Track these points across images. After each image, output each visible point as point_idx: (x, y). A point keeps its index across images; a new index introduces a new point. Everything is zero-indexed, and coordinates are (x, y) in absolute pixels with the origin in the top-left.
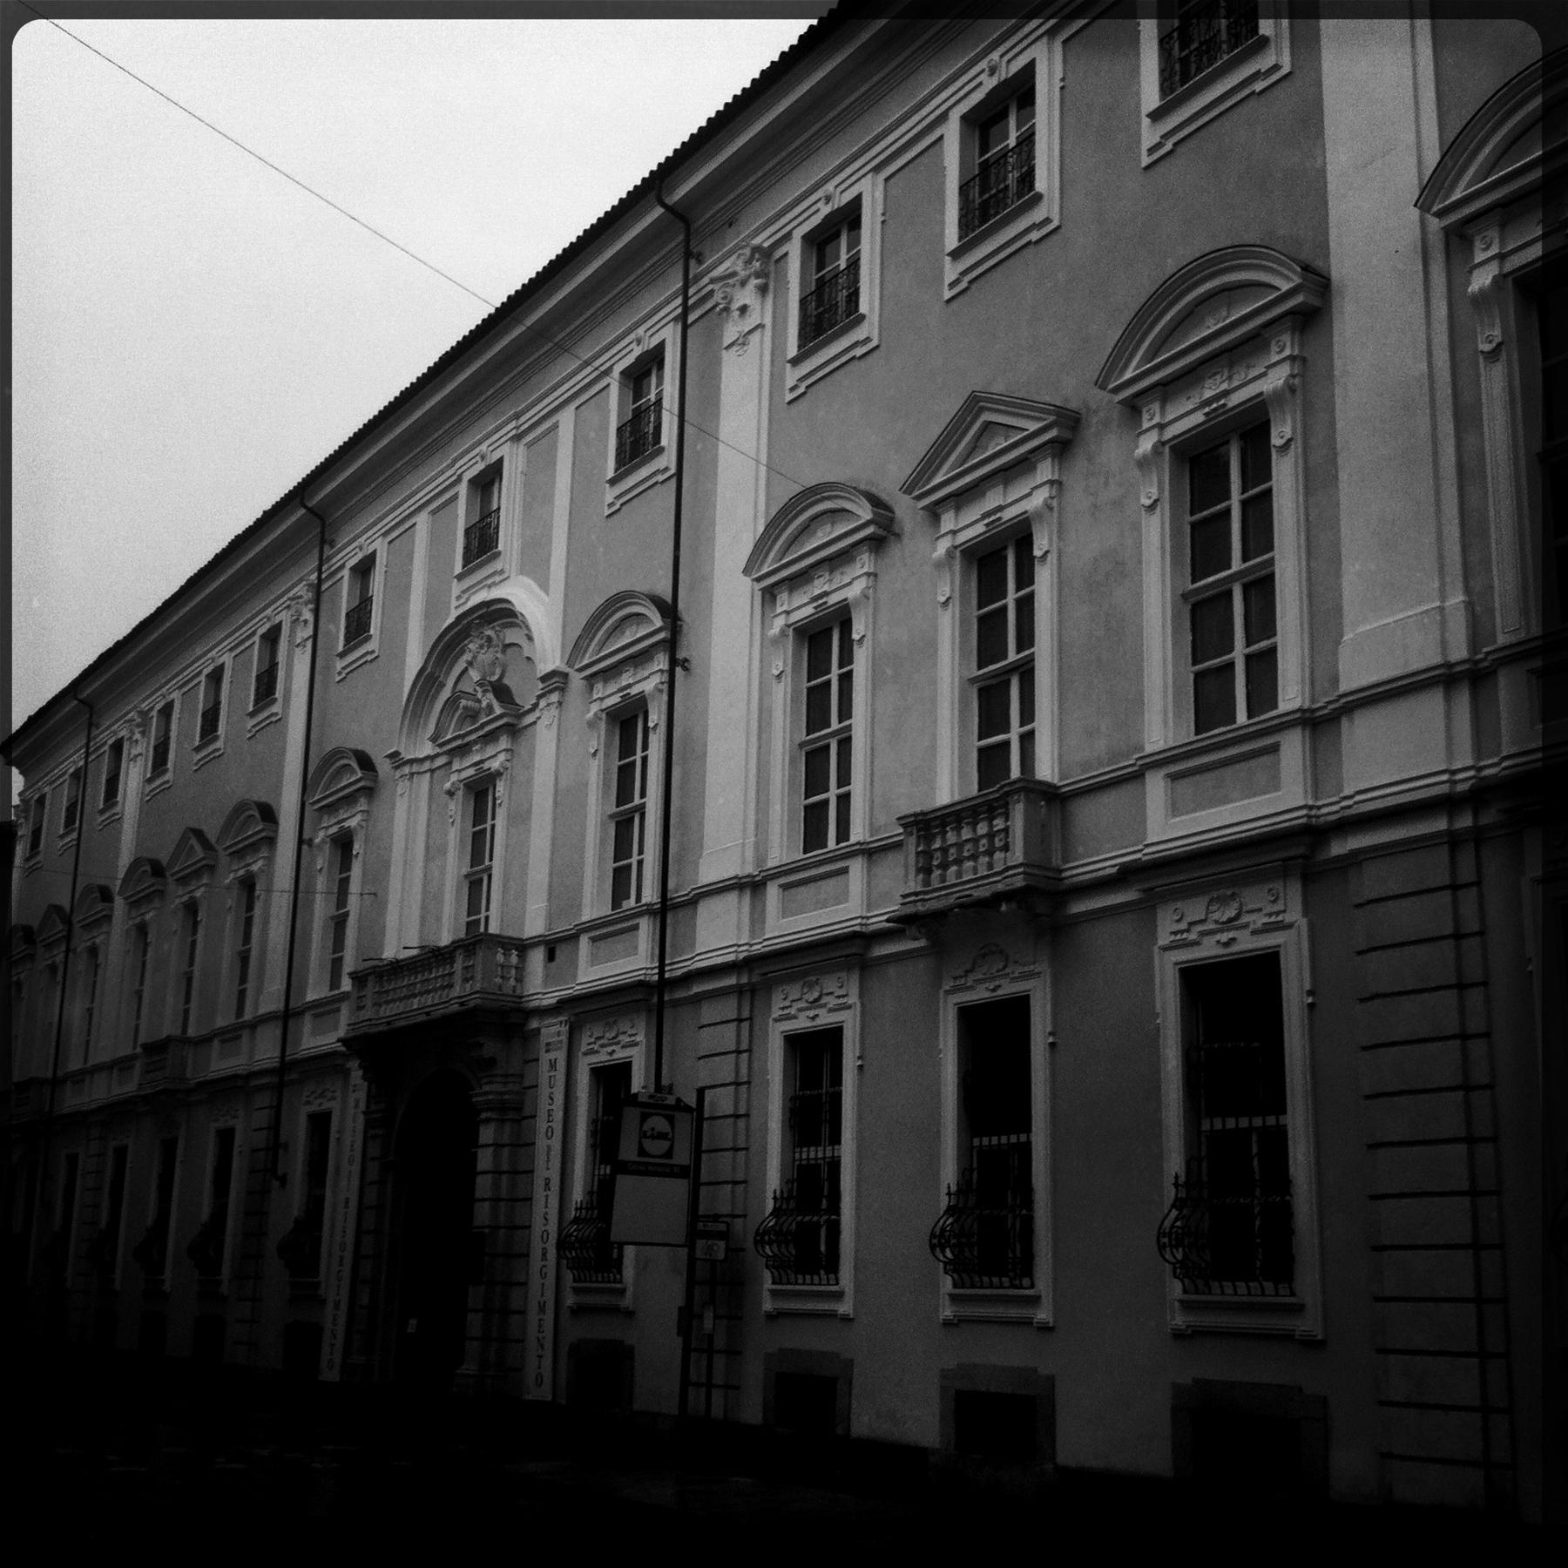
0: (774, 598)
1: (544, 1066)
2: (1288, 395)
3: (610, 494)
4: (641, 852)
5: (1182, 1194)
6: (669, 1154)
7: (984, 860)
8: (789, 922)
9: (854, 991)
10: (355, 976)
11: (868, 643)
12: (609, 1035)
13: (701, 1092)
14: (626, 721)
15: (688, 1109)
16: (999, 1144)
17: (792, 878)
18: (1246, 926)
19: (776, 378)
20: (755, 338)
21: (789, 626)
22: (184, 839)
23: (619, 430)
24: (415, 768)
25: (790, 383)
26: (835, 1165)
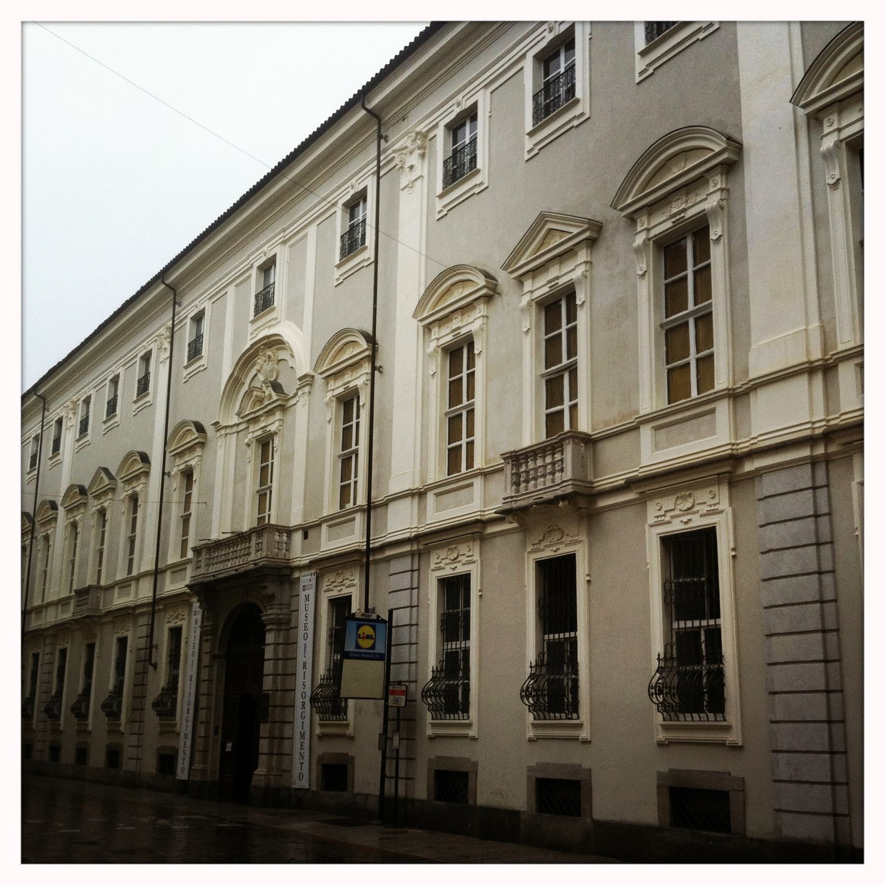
0: (430, 330)
4: (356, 476)
5: (662, 664)
8: (440, 514)
10: (76, 591)
12: (339, 580)
14: (347, 402)
15: (383, 621)
18: (698, 512)
22: (97, 473)
23: (342, 237)
24: (228, 431)
26: (466, 652)
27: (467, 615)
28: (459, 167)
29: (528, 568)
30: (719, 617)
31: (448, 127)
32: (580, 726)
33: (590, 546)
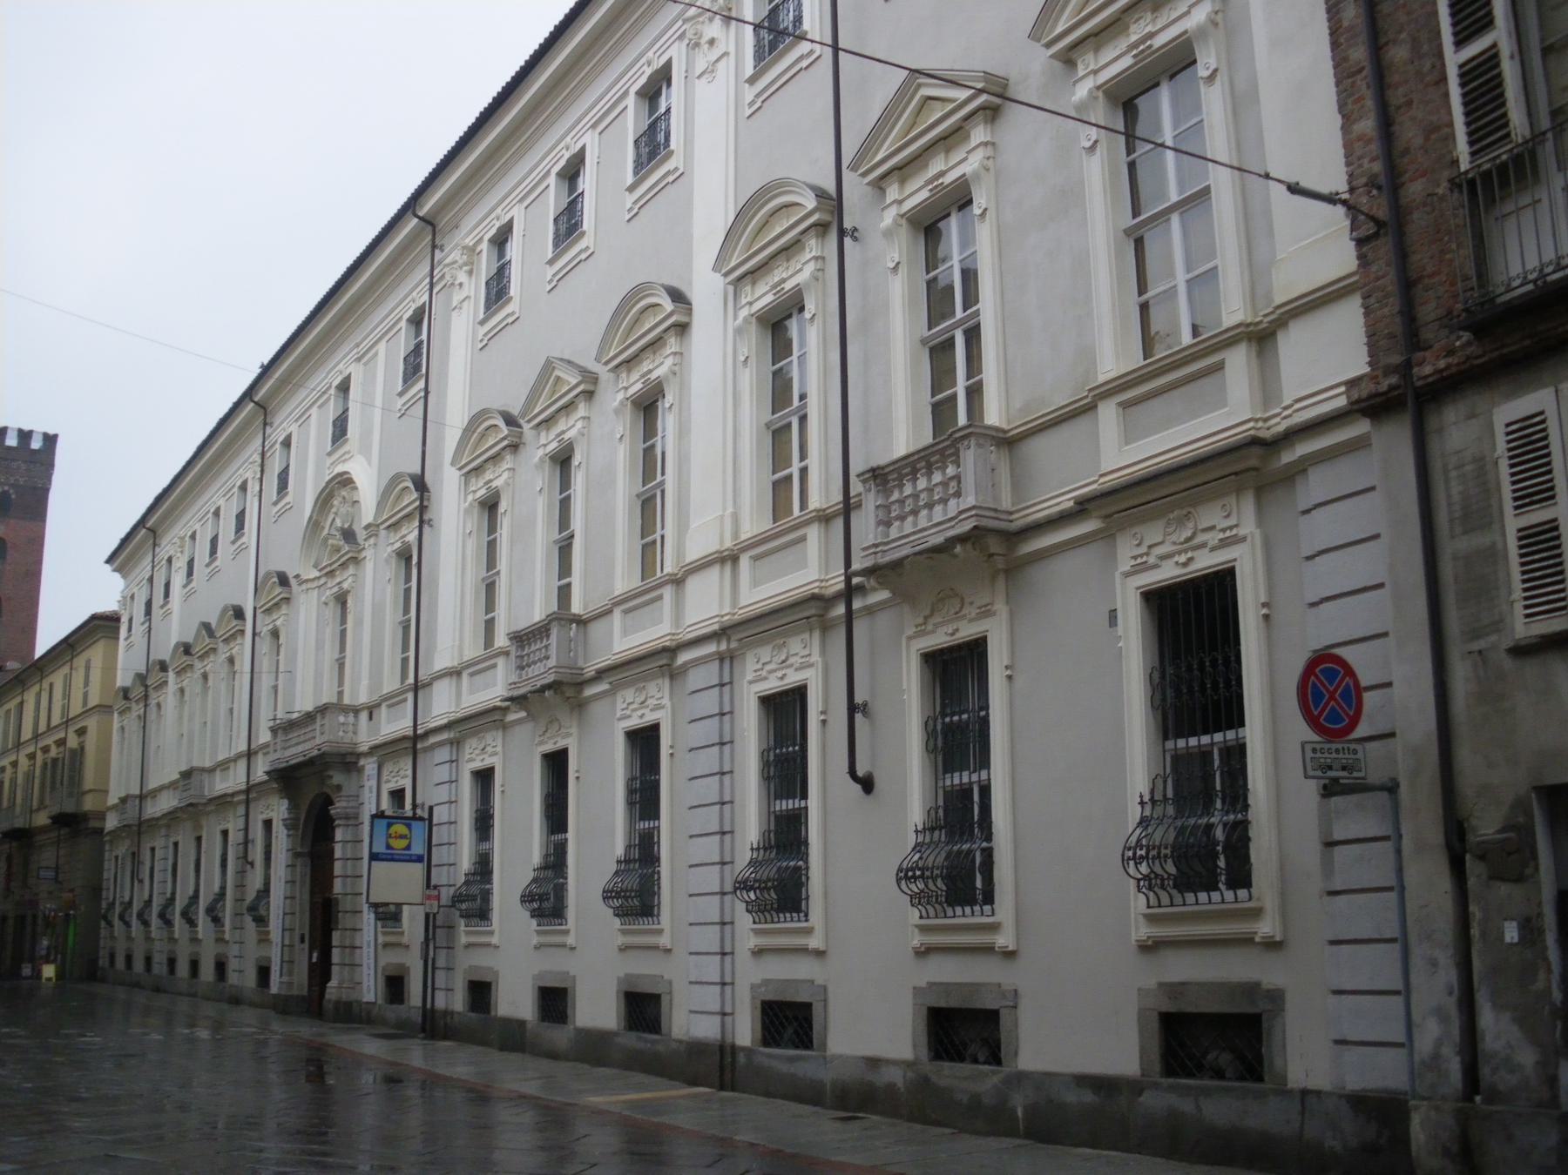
0: (882, 191)
1: (366, 789)
2: (983, 172)
3: (630, 199)
4: (803, 457)
6: (408, 847)
7: (924, 512)
8: (762, 590)
9: (499, 742)
11: (583, 466)
12: (639, 700)
13: (431, 808)
14: (404, 555)
15: (421, 819)
16: (1187, 747)
17: (764, 548)
18: (1203, 545)
19: (474, 333)
20: (722, 65)
21: (1098, 88)
23: (487, 283)
24: (310, 585)
25: (629, 205)
27: (985, 723)
28: (497, 291)
29: (908, 662)
30: (1242, 724)
31: (492, 241)
32: (660, 932)
33: (1012, 615)
